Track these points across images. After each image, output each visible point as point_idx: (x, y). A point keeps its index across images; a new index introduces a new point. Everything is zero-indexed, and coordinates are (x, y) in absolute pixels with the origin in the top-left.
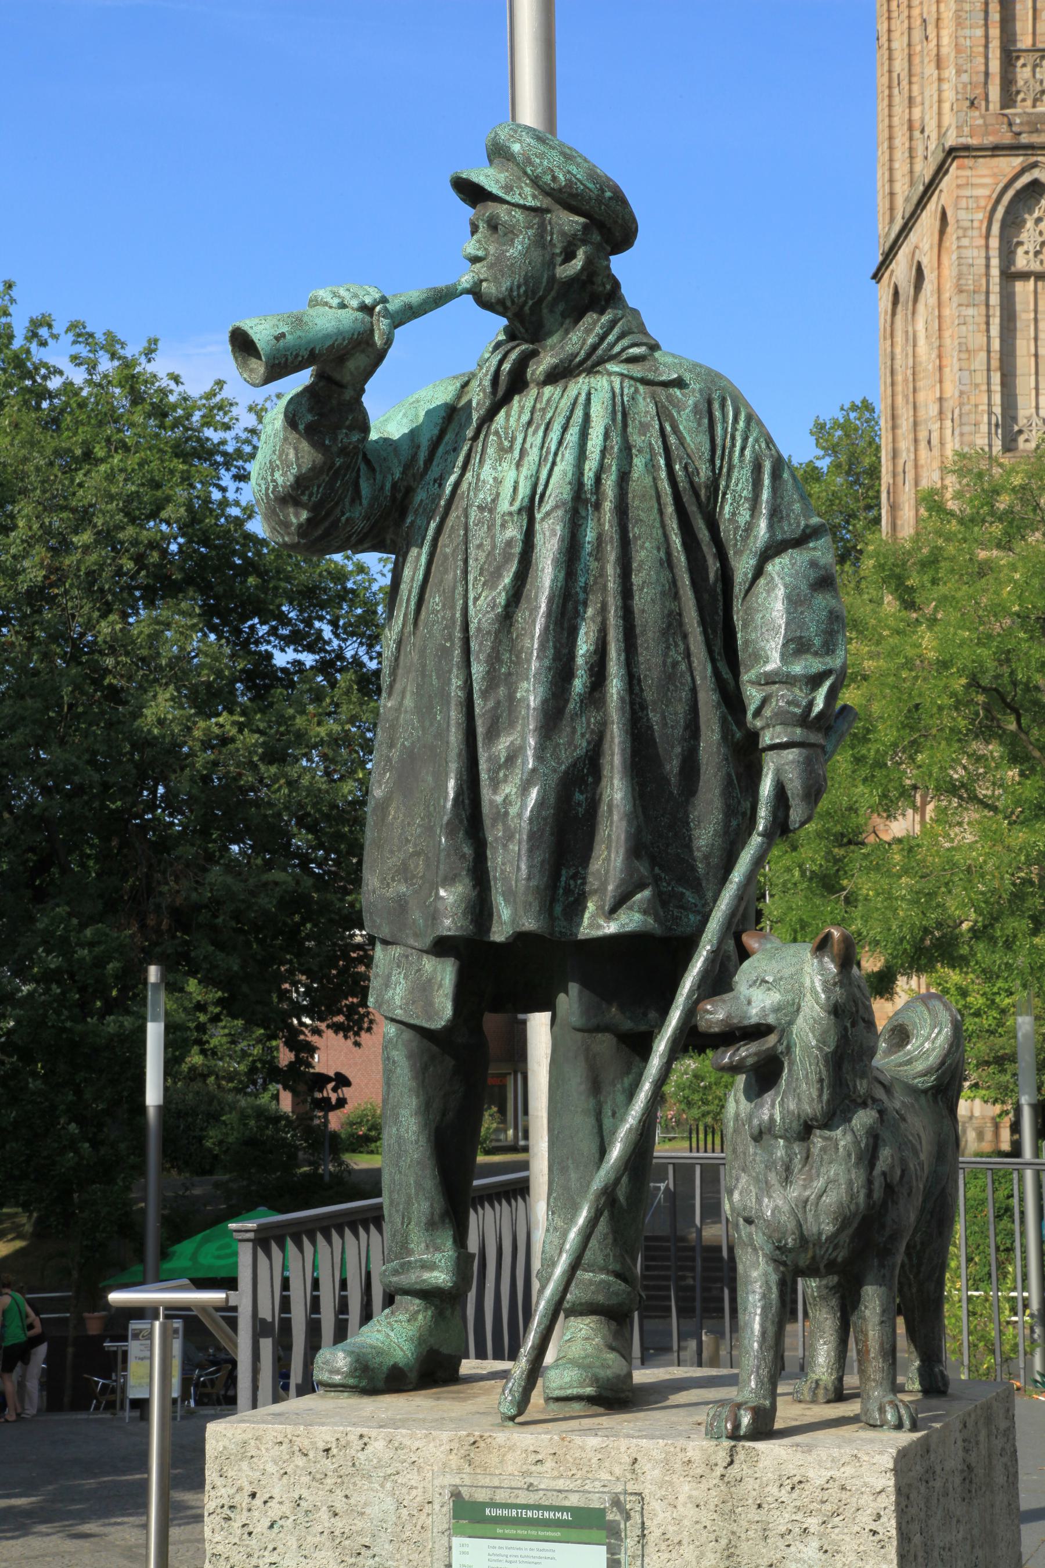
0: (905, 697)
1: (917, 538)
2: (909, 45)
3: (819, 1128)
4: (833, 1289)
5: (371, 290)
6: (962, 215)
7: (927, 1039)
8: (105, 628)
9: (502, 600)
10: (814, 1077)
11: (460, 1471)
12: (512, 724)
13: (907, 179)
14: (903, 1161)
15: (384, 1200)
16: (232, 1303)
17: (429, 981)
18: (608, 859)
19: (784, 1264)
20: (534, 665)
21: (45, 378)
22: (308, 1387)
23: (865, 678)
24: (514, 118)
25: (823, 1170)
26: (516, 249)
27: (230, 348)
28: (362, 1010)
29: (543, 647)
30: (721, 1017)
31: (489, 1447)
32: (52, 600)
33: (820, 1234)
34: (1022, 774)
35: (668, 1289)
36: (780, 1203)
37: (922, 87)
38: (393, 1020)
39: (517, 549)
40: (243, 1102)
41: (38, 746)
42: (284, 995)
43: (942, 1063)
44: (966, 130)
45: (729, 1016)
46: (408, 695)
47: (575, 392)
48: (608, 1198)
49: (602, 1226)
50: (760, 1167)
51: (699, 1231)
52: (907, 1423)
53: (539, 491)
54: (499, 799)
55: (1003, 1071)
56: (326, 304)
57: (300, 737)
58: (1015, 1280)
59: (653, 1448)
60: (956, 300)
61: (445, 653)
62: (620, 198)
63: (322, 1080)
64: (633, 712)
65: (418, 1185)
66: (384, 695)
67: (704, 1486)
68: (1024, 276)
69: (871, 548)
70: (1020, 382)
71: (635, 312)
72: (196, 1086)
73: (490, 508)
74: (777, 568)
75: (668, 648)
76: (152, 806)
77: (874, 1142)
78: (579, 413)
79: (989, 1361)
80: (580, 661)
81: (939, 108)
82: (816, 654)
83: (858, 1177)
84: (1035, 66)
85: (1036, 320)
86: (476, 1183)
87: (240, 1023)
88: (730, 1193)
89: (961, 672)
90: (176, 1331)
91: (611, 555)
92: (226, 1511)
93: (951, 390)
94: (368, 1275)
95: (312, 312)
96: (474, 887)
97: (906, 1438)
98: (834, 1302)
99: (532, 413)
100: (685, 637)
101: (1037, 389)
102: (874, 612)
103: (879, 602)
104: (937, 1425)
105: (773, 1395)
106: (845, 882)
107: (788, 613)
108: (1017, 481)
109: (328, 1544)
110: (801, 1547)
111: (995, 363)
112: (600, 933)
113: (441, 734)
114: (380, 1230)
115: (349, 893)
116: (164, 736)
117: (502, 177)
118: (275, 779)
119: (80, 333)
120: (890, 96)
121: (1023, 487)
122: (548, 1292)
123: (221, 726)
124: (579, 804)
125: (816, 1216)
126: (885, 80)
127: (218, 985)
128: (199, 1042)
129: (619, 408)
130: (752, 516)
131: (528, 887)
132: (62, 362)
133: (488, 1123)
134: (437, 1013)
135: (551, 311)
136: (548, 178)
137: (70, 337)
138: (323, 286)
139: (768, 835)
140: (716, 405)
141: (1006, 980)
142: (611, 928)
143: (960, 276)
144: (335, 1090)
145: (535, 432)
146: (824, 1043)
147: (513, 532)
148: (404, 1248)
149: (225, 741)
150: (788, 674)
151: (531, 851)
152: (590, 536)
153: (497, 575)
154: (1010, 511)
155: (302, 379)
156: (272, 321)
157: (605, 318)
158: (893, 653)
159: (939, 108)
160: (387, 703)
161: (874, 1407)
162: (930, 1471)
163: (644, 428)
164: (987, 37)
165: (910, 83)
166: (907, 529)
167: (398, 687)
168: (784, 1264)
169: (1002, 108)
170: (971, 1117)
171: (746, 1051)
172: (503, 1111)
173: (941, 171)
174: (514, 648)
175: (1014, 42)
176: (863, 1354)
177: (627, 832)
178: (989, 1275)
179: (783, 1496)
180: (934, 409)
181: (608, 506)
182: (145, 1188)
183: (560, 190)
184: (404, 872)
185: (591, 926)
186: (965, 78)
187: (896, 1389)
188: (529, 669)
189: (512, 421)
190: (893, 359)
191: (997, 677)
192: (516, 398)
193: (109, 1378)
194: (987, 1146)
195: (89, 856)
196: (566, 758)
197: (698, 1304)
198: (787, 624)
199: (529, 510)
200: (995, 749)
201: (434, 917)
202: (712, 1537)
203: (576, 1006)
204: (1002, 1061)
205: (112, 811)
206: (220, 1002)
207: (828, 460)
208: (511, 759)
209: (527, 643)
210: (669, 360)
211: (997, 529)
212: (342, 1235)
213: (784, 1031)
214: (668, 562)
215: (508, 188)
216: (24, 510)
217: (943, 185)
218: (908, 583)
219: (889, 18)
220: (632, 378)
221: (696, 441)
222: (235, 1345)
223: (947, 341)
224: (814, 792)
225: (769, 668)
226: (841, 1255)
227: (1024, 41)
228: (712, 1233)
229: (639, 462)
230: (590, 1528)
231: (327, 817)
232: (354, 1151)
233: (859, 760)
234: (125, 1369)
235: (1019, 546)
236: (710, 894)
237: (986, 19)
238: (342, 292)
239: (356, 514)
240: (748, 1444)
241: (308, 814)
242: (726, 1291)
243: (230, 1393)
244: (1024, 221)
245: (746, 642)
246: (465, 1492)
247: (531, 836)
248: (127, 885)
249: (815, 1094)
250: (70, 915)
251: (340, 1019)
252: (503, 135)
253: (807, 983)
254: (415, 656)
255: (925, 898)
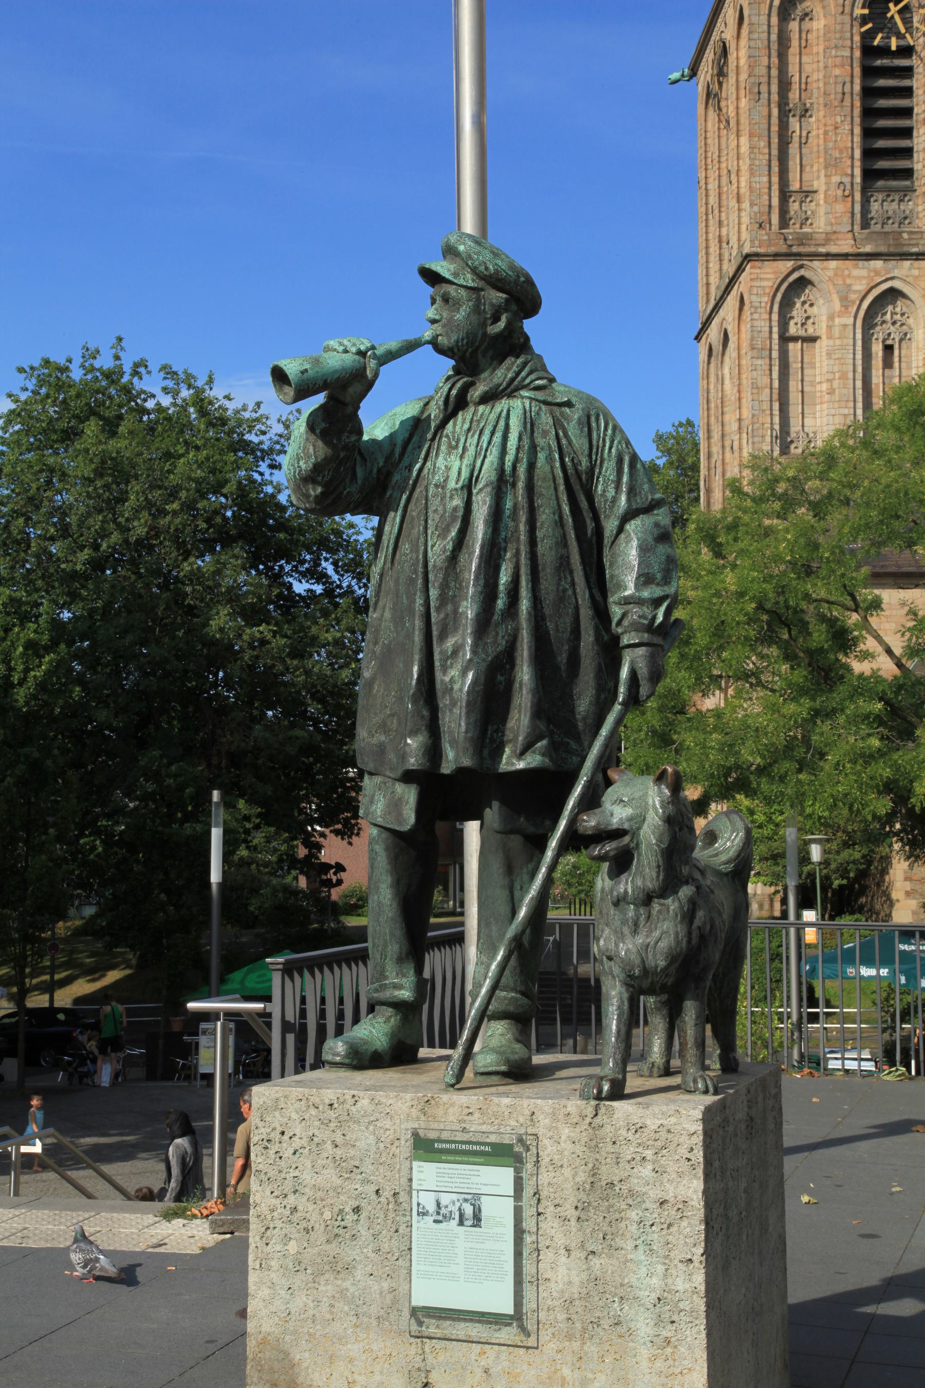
0: (715, 615)
1: (724, 511)
2: (719, 187)
3: (658, 897)
4: (665, 1003)
5: (365, 341)
6: (754, 298)
7: (729, 840)
8: (186, 567)
9: (450, 547)
10: (654, 864)
11: (418, 1119)
12: (456, 629)
13: (718, 274)
14: (712, 920)
15: (369, 944)
16: (268, 1010)
17: (400, 799)
18: (519, 719)
19: (632, 986)
20: (471, 591)
21: (145, 400)
22: (318, 1064)
23: (689, 603)
24: (459, 229)
25: (659, 925)
26: (461, 315)
27: (271, 379)
28: (353, 822)
29: (477, 578)
30: (593, 824)
31: (437, 1104)
32: (151, 548)
33: (657, 967)
34: (792, 668)
35: (555, 1006)
36: (631, 947)
37: (728, 214)
38: (375, 825)
39: (460, 513)
40: (275, 881)
41: (142, 645)
42: (301, 811)
43: (738, 856)
44: (757, 243)
45: (598, 824)
46: (387, 610)
47: (499, 410)
48: (517, 945)
49: (513, 961)
50: (618, 923)
51: (576, 968)
52: (711, 1090)
53: (475, 474)
54: (447, 679)
55: (777, 864)
56: (335, 350)
57: (314, 639)
58: (781, 1000)
59: (546, 1105)
60: (749, 354)
61: (412, 581)
62: (530, 282)
63: (326, 867)
64: (536, 622)
65: (392, 934)
66: (371, 609)
67: (578, 1130)
68: (795, 339)
69: (694, 517)
70: (792, 409)
71: (540, 357)
72: (244, 870)
73: (442, 486)
74: (633, 527)
75: (560, 579)
76: (215, 685)
77: (693, 906)
78: (502, 423)
79: (763, 1053)
80: (501, 588)
81: (739, 228)
82: (658, 584)
83: (682, 930)
84: (801, 202)
85: (802, 368)
86: (429, 934)
87: (272, 829)
88: (598, 940)
89: (752, 599)
90: (231, 1030)
91: (523, 517)
92: (265, 1143)
93: (746, 413)
94: (358, 995)
95: (326, 355)
96: (430, 737)
97: (710, 1099)
98: (665, 1012)
99: (471, 423)
100: (571, 572)
101: (803, 413)
102: (695, 559)
103: (699, 553)
104: (731, 1091)
105: (624, 1072)
106: (675, 737)
107: (640, 557)
108: (791, 473)
109: (332, 1165)
110: (641, 1169)
111: (775, 396)
112: (513, 768)
113: (409, 636)
114: (365, 965)
115: (346, 744)
116: (223, 639)
117: (452, 267)
118: (297, 668)
119: (168, 372)
120: (707, 220)
121: (794, 478)
122: (477, 1004)
123: (262, 633)
124: (500, 683)
125: (654, 955)
126: (703, 209)
127: (259, 804)
128: (245, 841)
129: (528, 420)
130: (616, 493)
131: (466, 738)
132: (157, 391)
133: (437, 897)
134: (405, 821)
135: (484, 356)
136: (482, 268)
137: (162, 374)
138: (333, 339)
139: (625, 704)
140: (593, 419)
141: (779, 803)
142: (521, 765)
143: (752, 339)
144: (335, 874)
145: (473, 436)
146: (661, 842)
147: (458, 502)
148: (382, 975)
149: (263, 642)
150: (640, 598)
151: (468, 713)
152: (509, 505)
153: (447, 530)
154: (785, 494)
155: (319, 399)
156: (300, 361)
157: (519, 361)
158: (706, 587)
159: (739, 228)
160: (373, 615)
161: (690, 1079)
162: (726, 1121)
163: (545, 433)
164: (770, 182)
165: (720, 212)
166: (717, 506)
167: (381, 604)
168: (632, 986)
169: (780, 228)
170: (755, 895)
171: (609, 847)
172: (446, 889)
173: (740, 270)
174: (458, 578)
175: (788, 186)
176: (683, 1045)
177: (532, 702)
178: (766, 998)
179: (630, 1135)
180: (735, 426)
181: (521, 485)
182: (210, 937)
183: (491, 276)
184: (384, 727)
185: (507, 763)
186: (756, 209)
187: (705, 1068)
188: (467, 592)
189: (458, 428)
190: (708, 393)
191: (777, 603)
192: (460, 413)
193: (186, 1059)
194: (765, 913)
195: (174, 718)
196: (492, 651)
197: (574, 1016)
198: (639, 564)
199: (468, 487)
200: (774, 651)
201: (403, 757)
202: (583, 1162)
203: (497, 816)
204: (776, 857)
205: (189, 688)
206: (259, 815)
207: (664, 460)
208: (455, 653)
209: (466, 575)
210: (562, 389)
211: (777, 506)
212: (340, 968)
213: (634, 833)
214: (561, 522)
215: (456, 275)
216: (135, 487)
217: (741, 279)
218: (718, 540)
219: (706, 169)
220: (537, 400)
221: (579, 442)
222: (270, 1038)
223: (744, 382)
224: (656, 675)
225: (627, 593)
226: (670, 981)
227: (795, 186)
228: (585, 969)
229: (541, 456)
230: (503, 1156)
231: (332, 694)
232: (348, 914)
233: (683, 656)
234: (197, 1054)
235: (791, 517)
236: (586, 744)
237: (770, 171)
238: (346, 342)
239: (353, 490)
240: (607, 1103)
241: (318, 691)
242: (593, 1007)
243: (266, 1070)
244: (795, 303)
245: (612, 576)
246: (421, 1133)
247: (468, 704)
248: (198, 738)
249: (654, 875)
250: (161, 756)
251: (339, 826)
252: (453, 239)
253: (651, 802)
254: (392, 584)
255: (729, 748)
